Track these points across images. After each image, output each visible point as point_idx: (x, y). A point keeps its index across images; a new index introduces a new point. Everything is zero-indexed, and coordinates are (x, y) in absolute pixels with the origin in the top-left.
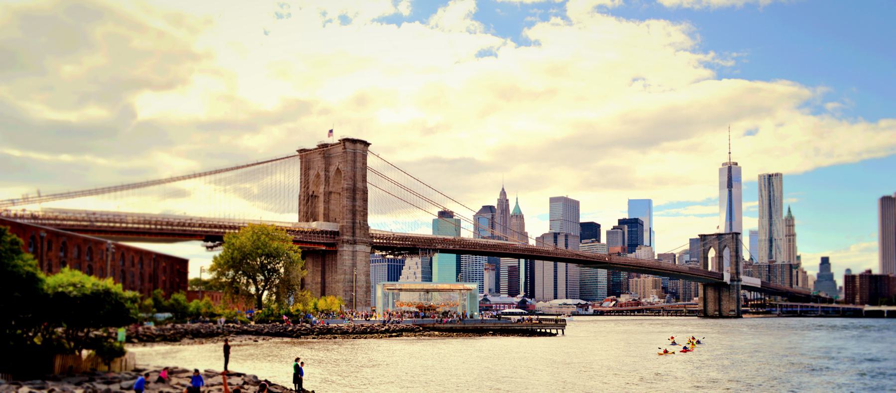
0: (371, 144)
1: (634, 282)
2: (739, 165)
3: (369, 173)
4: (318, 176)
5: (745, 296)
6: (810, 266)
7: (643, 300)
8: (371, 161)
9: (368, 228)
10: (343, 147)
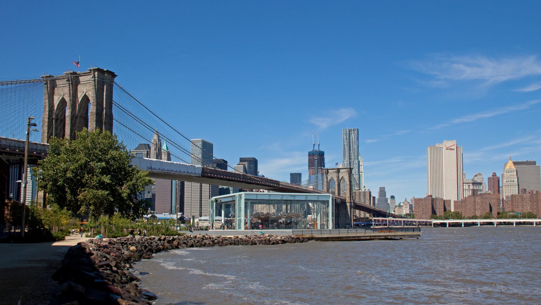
0: (117, 76)
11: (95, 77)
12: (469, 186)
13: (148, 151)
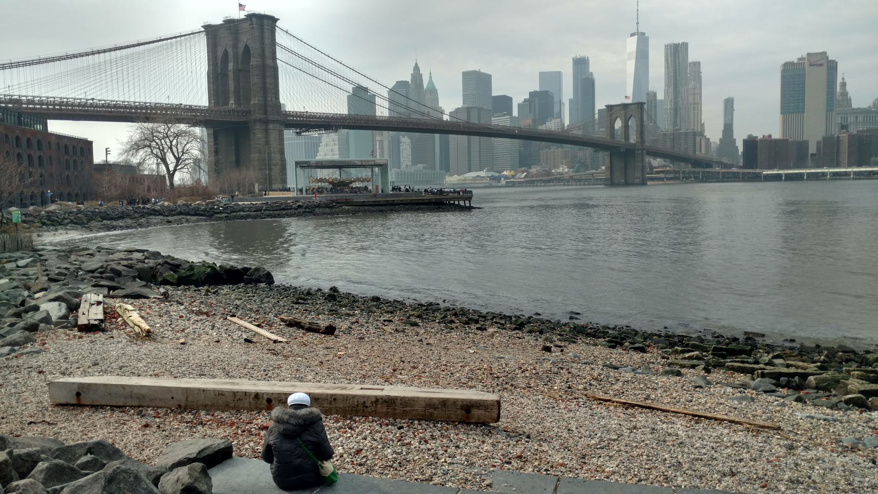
0: (279, 19)
2: (646, 35)
3: (278, 49)
4: (226, 53)
6: (714, 133)
7: (553, 171)
8: (280, 38)
10: (250, 22)
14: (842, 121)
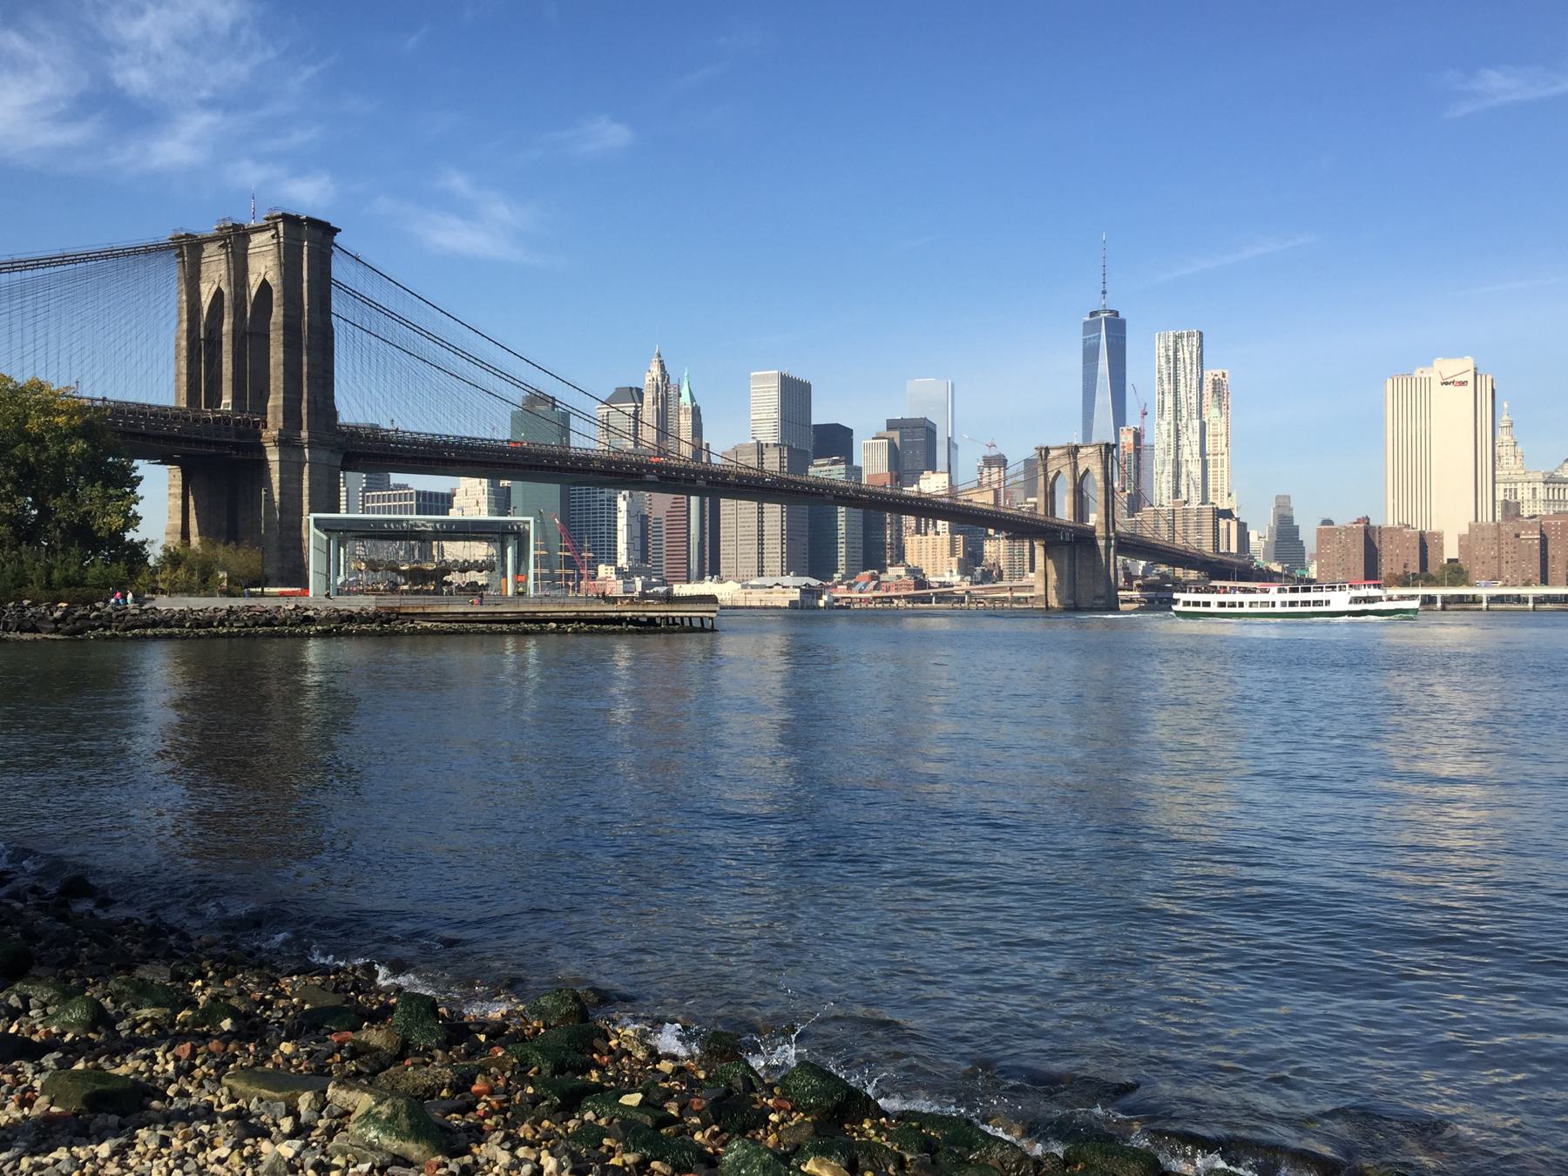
0: (340, 230)
1: (915, 542)
2: (1121, 316)
3: (335, 294)
4: (219, 294)
5: (1125, 568)
9: (335, 414)
11: (279, 237)
12: (1534, 489)
13: (636, 407)
14: (1505, 496)
